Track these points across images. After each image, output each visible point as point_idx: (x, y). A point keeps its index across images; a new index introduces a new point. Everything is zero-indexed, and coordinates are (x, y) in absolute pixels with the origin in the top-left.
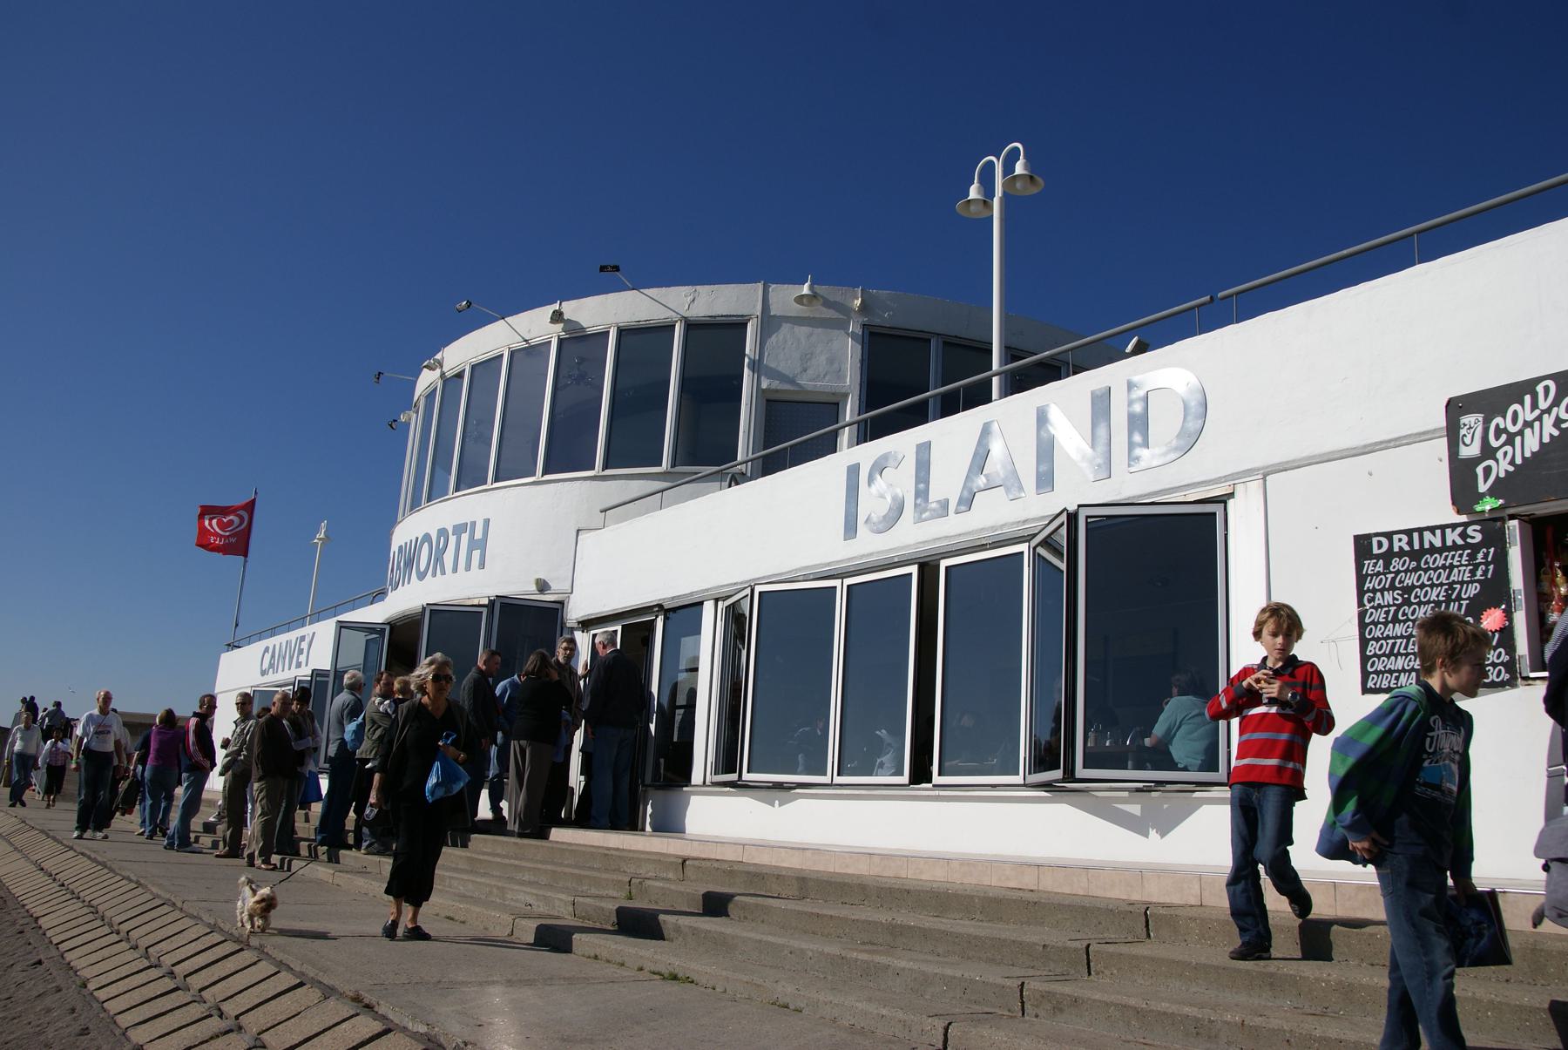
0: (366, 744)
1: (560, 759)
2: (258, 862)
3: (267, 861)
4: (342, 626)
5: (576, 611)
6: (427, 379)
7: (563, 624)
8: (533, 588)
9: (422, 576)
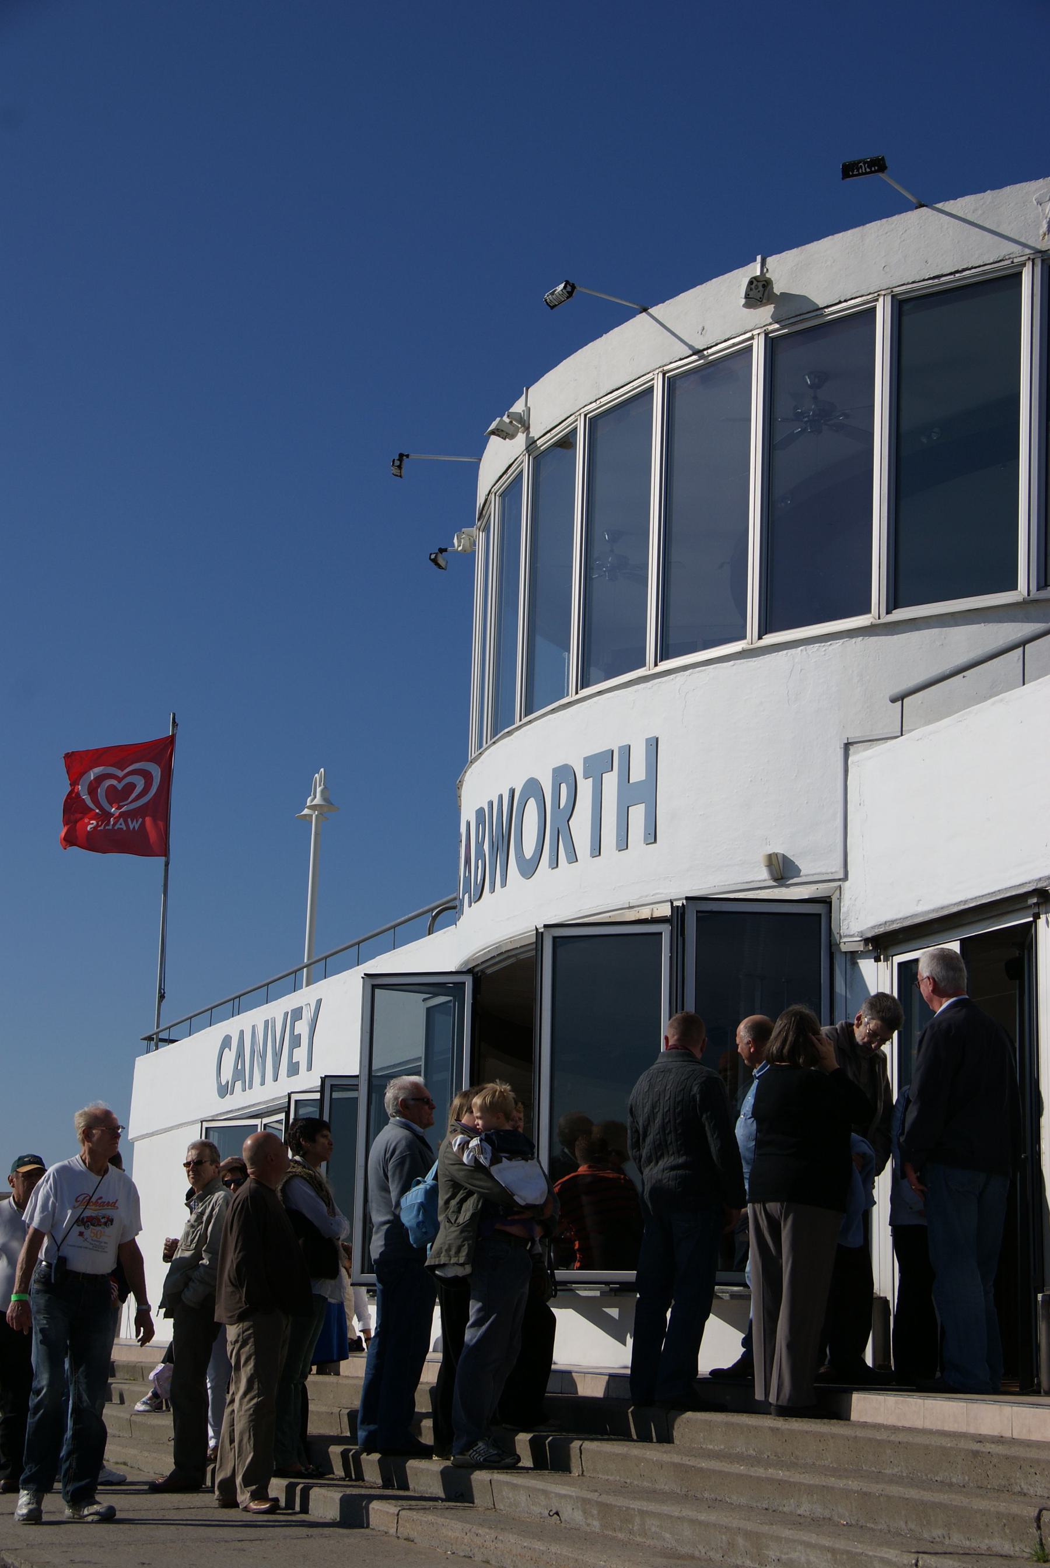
0: (446, 1236)
1: (859, 1242)
2: (243, 1497)
3: (260, 1495)
4: (375, 983)
5: (859, 916)
6: (499, 457)
7: (833, 947)
8: (763, 874)
9: (529, 869)
